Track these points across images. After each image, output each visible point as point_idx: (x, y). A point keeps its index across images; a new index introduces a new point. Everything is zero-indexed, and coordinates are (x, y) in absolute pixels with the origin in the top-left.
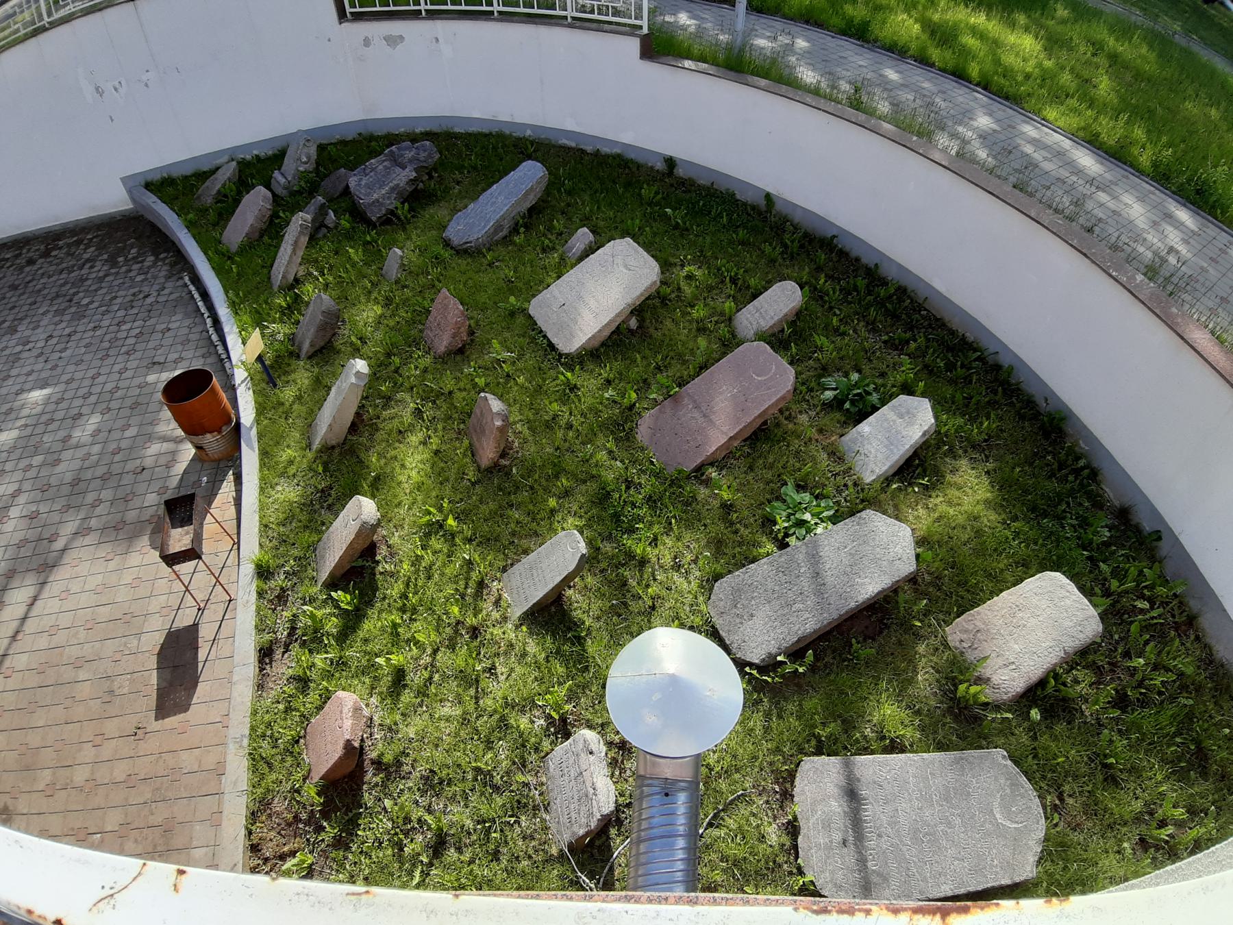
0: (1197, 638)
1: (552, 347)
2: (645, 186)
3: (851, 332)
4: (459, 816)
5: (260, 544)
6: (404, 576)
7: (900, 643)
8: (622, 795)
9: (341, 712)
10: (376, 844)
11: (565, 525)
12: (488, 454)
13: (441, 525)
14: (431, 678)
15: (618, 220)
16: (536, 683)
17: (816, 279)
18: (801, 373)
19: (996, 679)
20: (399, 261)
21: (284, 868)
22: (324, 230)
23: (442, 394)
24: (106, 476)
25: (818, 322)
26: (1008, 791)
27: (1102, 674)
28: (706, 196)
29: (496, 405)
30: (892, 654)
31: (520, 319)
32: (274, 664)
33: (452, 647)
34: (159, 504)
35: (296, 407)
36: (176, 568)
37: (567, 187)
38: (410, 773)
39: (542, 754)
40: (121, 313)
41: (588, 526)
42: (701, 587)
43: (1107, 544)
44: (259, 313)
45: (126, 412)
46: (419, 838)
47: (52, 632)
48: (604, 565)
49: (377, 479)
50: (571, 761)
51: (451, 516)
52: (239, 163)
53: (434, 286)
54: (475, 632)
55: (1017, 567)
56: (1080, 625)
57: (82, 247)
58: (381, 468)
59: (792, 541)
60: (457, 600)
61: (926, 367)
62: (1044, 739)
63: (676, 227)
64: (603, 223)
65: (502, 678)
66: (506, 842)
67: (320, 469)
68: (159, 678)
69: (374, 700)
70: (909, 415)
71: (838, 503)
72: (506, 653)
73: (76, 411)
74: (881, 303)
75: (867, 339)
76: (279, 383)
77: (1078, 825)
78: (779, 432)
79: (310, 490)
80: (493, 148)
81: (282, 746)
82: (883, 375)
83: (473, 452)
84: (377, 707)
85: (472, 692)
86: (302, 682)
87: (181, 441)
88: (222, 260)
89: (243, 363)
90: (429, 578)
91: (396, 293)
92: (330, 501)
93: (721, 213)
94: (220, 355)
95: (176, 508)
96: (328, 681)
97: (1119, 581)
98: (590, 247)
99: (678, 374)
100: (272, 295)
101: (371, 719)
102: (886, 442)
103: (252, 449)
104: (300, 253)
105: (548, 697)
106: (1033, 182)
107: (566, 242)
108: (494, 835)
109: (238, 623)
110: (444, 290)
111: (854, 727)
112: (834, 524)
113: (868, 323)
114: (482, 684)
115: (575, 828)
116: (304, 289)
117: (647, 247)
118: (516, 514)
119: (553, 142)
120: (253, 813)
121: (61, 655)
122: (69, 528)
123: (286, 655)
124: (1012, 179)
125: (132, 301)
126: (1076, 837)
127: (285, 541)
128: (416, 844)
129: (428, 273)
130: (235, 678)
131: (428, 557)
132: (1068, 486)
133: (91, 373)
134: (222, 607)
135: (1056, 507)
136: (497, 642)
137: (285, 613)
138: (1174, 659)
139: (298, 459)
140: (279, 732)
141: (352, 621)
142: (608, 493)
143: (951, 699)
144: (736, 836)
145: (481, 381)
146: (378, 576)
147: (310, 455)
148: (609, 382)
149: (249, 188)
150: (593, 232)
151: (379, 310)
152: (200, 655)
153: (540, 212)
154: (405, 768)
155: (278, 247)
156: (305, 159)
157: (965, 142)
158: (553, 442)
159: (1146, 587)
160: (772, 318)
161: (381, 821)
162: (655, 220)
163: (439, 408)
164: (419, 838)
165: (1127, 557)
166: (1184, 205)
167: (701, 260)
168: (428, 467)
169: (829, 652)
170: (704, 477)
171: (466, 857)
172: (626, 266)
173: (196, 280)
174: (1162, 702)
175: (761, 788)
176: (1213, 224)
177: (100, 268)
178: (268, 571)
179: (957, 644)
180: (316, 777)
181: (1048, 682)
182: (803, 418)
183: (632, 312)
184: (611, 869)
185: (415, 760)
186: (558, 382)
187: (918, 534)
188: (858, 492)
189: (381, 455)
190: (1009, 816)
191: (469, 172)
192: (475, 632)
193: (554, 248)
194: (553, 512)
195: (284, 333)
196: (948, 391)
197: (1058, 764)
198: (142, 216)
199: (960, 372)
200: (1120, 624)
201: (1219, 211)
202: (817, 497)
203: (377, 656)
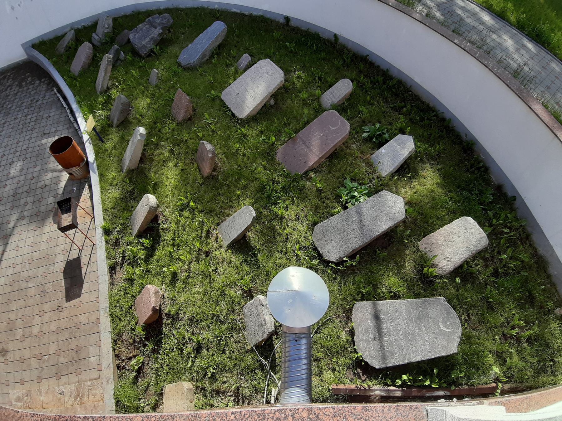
0: (530, 244)
1: (233, 115)
2: (275, 31)
4: (206, 335)
5: (104, 218)
7: (398, 250)
9: (149, 294)
10: (171, 350)
12: (207, 170)
13: (187, 205)
14: (189, 275)
16: (237, 275)
17: (359, 77)
19: (441, 265)
20: (156, 75)
21: (131, 364)
22: (119, 62)
23: (182, 141)
24: (28, 191)
25: (360, 98)
26: (446, 315)
27: (487, 261)
29: (208, 147)
31: (217, 102)
33: (197, 260)
35: (113, 151)
37: (237, 33)
38: (183, 318)
39: (241, 306)
41: (256, 202)
42: (309, 228)
43: (491, 203)
45: (34, 159)
46: (189, 346)
47: (14, 265)
48: (264, 220)
49: (155, 184)
50: (254, 309)
52: (75, 30)
54: (207, 254)
55: (451, 214)
56: (479, 241)
59: (349, 205)
60: (198, 240)
61: (411, 119)
62: (461, 291)
63: (291, 52)
64: (255, 51)
65: (221, 273)
66: (228, 345)
67: (128, 181)
68: (65, 283)
69: (164, 287)
70: (403, 144)
71: (370, 186)
72: (222, 262)
73: (10, 161)
75: (383, 107)
76: (105, 140)
80: (200, 15)
81: (124, 310)
82: (391, 124)
83: (199, 169)
84: (165, 290)
85: (208, 280)
86: (131, 281)
87: (62, 171)
88: (71, 81)
89: (86, 131)
90: (184, 230)
92: (134, 197)
93: (313, 44)
94: (75, 128)
96: (142, 280)
99: (295, 127)
100: (97, 96)
102: (392, 157)
103: (95, 173)
104: (108, 75)
105: (242, 281)
107: (238, 61)
108: (222, 342)
109: (98, 256)
110: (179, 89)
111: (378, 288)
113: (383, 98)
114: (212, 277)
115: (258, 338)
116: (112, 92)
117: (277, 63)
120: (115, 341)
121: (19, 276)
122: (14, 218)
123: (122, 269)
124: (453, 27)
126: (474, 333)
127: (115, 216)
128: (189, 349)
129: (171, 81)
130: (100, 282)
133: (16, 141)
134: (90, 248)
135: (469, 185)
137: (119, 250)
138: (520, 254)
139: (117, 177)
141: (150, 252)
142: (264, 186)
143: (421, 274)
144: (327, 337)
145: (200, 134)
147: (123, 175)
148: (262, 132)
149: (81, 42)
150: (250, 56)
152: (82, 271)
154: (180, 316)
155: (98, 72)
156: (107, 26)
157: (429, 8)
159: (508, 222)
160: (338, 97)
161: (172, 340)
162: (281, 49)
164: (189, 346)
165: (500, 208)
166: (531, 41)
167: (304, 68)
168: (179, 178)
170: (308, 177)
171: (211, 353)
172: (267, 73)
173: (60, 91)
174: (514, 273)
176: (544, 50)
177: (15, 89)
178: (109, 231)
179: (423, 249)
180: (141, 322)
182: (354, 147)
183: (271, 96)
184: (274, 354)
185: (185, 312)
187: (406, 199)
188: (379, 181)
189: (156, 173)
190: (446, 326)
191: (188, 28)
192: (207, 254)
193: (232, 65)
194: (239, 196)
195: (105, 116)
196: (420, 131)
198: (32, 61)
199: (426, 122)
200: (496, 239)
201: (546, 45)
202: (360, 184)
203: (164, 267)
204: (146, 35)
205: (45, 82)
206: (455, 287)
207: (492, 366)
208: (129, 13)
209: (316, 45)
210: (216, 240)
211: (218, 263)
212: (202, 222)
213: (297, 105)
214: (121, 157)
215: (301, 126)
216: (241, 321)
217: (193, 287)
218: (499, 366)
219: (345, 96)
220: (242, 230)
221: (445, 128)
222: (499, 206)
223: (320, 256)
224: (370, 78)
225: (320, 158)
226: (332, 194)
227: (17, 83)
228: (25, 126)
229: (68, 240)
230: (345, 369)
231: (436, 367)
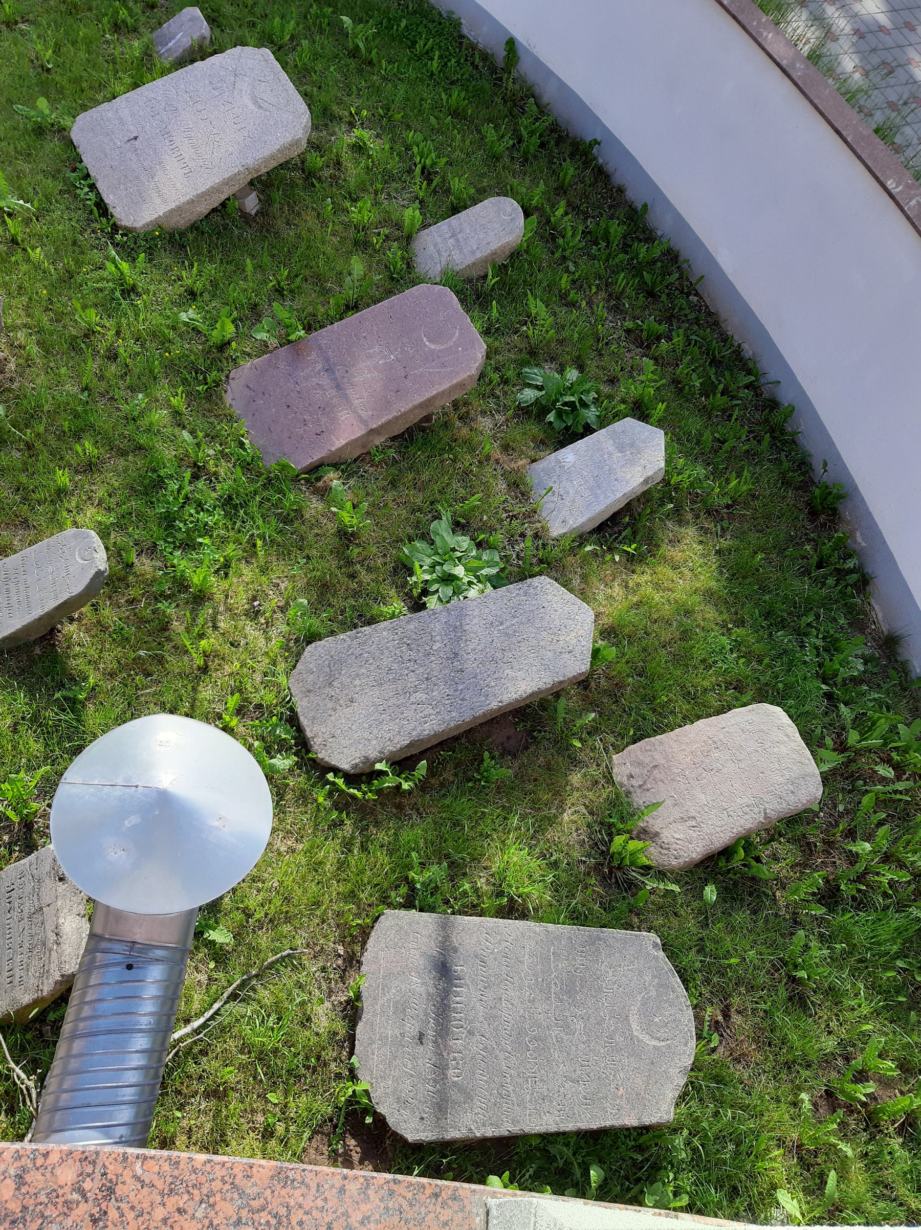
1: (102, 208)
3: (584, 303)
7: (549, 767)
11: (79, 519)
18: (497, 352)
19: (667, 835)
26: (653, 993)
28: (415, 12)
30: (535, 780)
31: (53, 145)
41: (120, 526)
42: (287, 648)
48: (134, 592)
50: (28, 889)
55: (727, 689)
56: (793, 783)
59: (432, 602)
62: (717, 929)
63: (354, 53)
74: (636, 269)
77: (743, 1055)
78: (446, 436)
82: (612, 381)
97: (861, 734)
98: (200, 47)
99: (310, 309)
106: (908, 130)
107: (160, 24)
111: (465, 874)
112: (495, 587)
124: (879, 117)
126: (739, 1071)
132: (824, 592)
144: (269, 1016)
150: (211, 20)
157: (829, 34)
159: (896, 748)
160: (473, 252)
162: (321, 31)
165: (880, 703)
169: (451, 766)
170: (320, 484)
174: (886, 908)
175: (318, 948)
179: (625, 780)
181: (736, 852)
182: (485, 424)
183: (251, 183)
186: (105, 274)
187: (605, 620)
190: (648, 1027)
193: (135, 30)
196: (694, 424)
197: (730, 966)
199: (720, 400)
200: (850, 792)
202: (479, 545)
206: (700, 912)
207: (775, 1189)
209: (441, 57)
213: (335, 240)
218: (801, 1195)
219: (494, 253)
220: (46, 610)
221: (772, 431)
222: (876, 696)
223: (302, 744)
224: (586, 219)
225: (372, 431)
226: (385, 555)
230: (306, 1136)
231: (601, 1162)
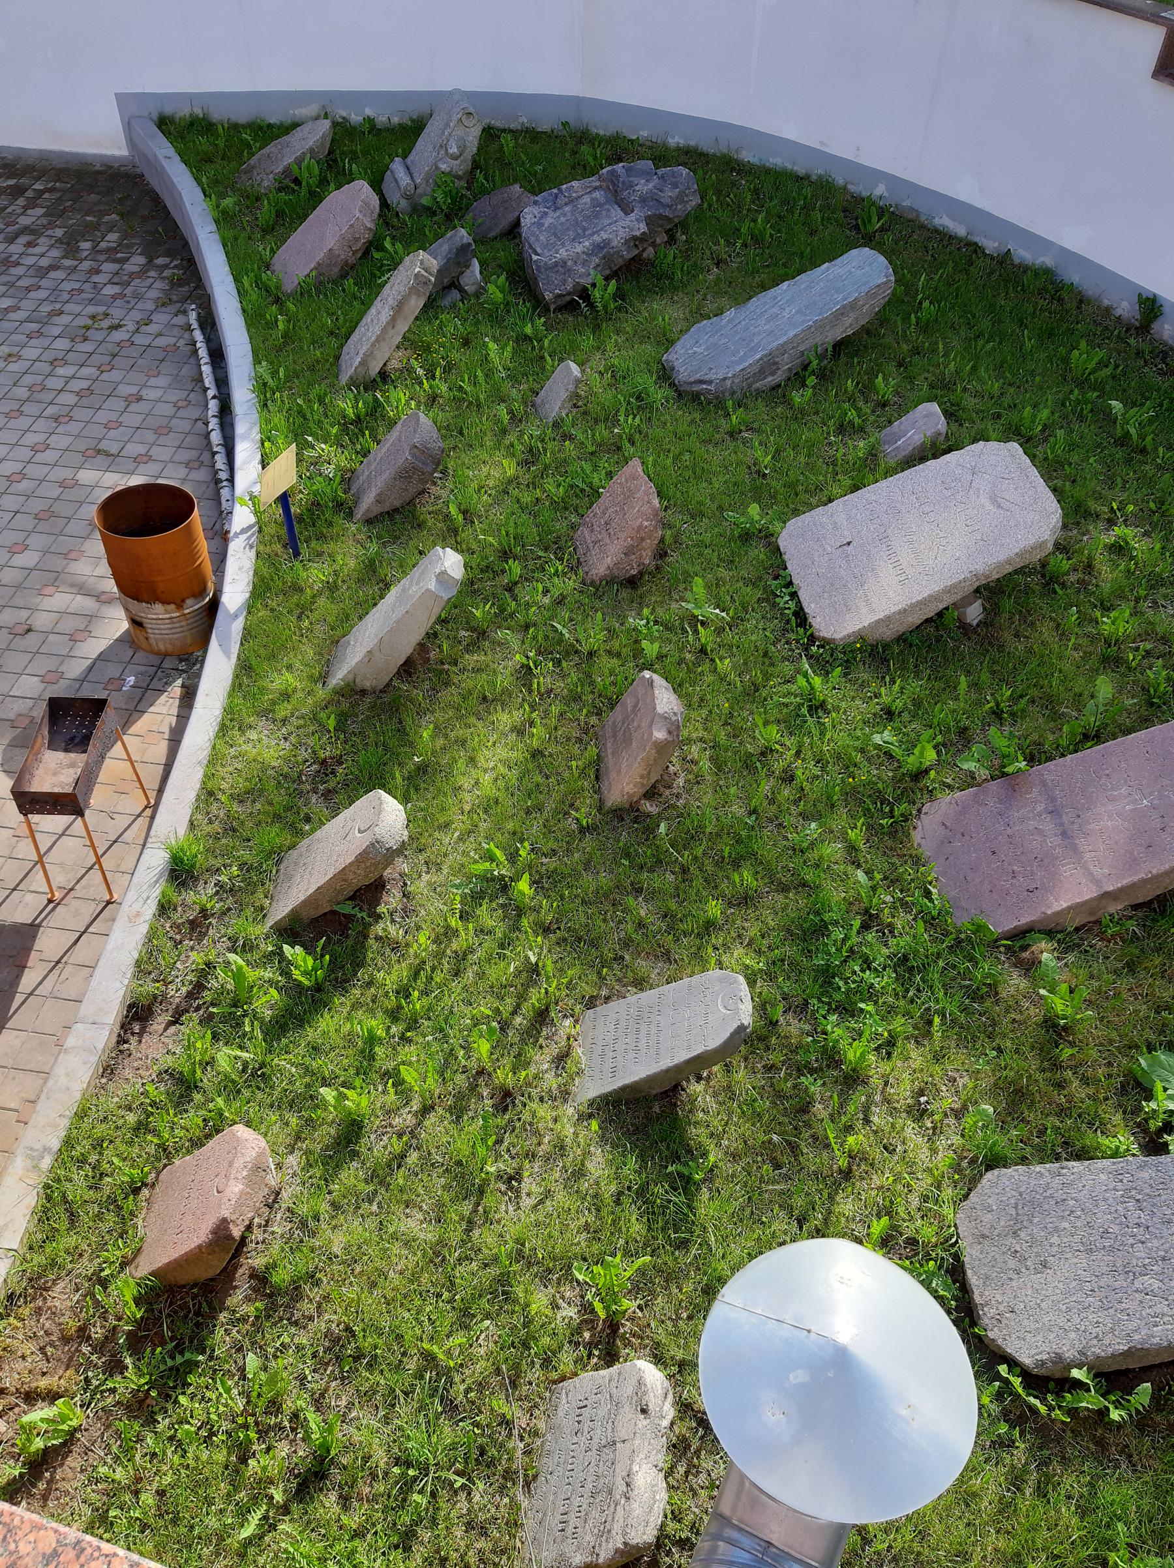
1: (801, 617)
5: (191, 823)
6: (416, 956)
8: (676, 1517)
9: (231, 1165)
11: (724, 958)
14: (403, 1156)
15: (1006, 401)
20: (571, 387)
21: (26, 1419)
22: (455, 295)
23: (576, 652)
29: (666, 700)
31: (758, 552)
32: (146, 1038)
33: (458, 1112)
34: (39, 699)
35: (322, 601)
36: (34, 818)
38: (311, 1319)
39: (554, 1375)
40: (63, 344)
41: (771, 977)
42: (957, 1168)
44: (304, 417)
48: (776, 1057)
49: (422, 769)
50: (603, 1411)
51: (526, 876)
52: (335, 124)
53: (619, 449)
54: (505, 1099)
57: (21, 201)
58: (434, 752)
60: (491, 1031)
63: (1123, 441)
64: (973, 401)
65: (527, 1202)
66: (434, 1522)
67: (332, 723)
76: (304, 549)
79: (304, 754)
81: (107, 1191)
83: (597, 771)
84: (294, 1175)
87: (109, 602)
89: (252, 498)
91: (550, 445)
94: (216, 472)
95: (66, 715)
96: (227, 1101)
98: (933, 444)
101: (278, 1194)
103: (227, 653)
104: (403, 327)
105: (597, 1269)
107: (890, 422)
108: (416, 1497)
109: (109, 947)
110: (635, 463)
114: (489, 1201)
115: (569, 1548)
117: (1050, 469)
118: (643, 910)
119: (923, 218)
123: (173, 1029)
125: (88, 328)
127: (234, 830)
130: (70, 1042)
131: (465, 937)
134: (90, 909)
136: (537, 1133)
137: (194, 955)
139: (300, 694)
140: (111, 1163)
145: (651, 649)
146: (371, 942)
147: (321, 693)
149: (344, 178)
150: (948, 414)
151: (510, 468)
153: (856, 353)
155: (367, 305)
156: (454, 150)
158: (749, 798)
161: (228, 1391)
162: (1081, 418)
163: (563, 676)
168: (513, 775)
170: (1025, 955)
171: (352, 1521)
172: (994, 500)
173: (209, 323)
177: (45, 251)
180: (146, 1266)
185: (326, 1298)
186: (793, 688)
191: (745, 245)
192: (505, 1099)
193: (862, 429)
194: (709, 926)
195: (338, 468)
203: (325, 1083)
204: (585, 229)
205: (167, 273)
208: (545, 127)
210: (561, 1059)
211: (531, 1156)
212: (535, 970)
214: (339, 632)
215: (1064, 742)
216: (527, 1439)
217: (399, 1210)
220: (676, 1061)
225: (1106, 895)
227: (59, 232)
228: (37, 396)
229: (26, 850)
